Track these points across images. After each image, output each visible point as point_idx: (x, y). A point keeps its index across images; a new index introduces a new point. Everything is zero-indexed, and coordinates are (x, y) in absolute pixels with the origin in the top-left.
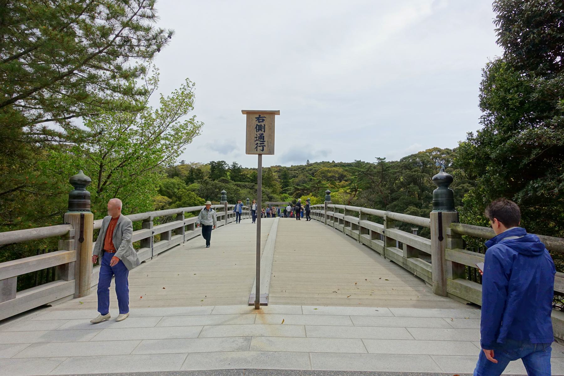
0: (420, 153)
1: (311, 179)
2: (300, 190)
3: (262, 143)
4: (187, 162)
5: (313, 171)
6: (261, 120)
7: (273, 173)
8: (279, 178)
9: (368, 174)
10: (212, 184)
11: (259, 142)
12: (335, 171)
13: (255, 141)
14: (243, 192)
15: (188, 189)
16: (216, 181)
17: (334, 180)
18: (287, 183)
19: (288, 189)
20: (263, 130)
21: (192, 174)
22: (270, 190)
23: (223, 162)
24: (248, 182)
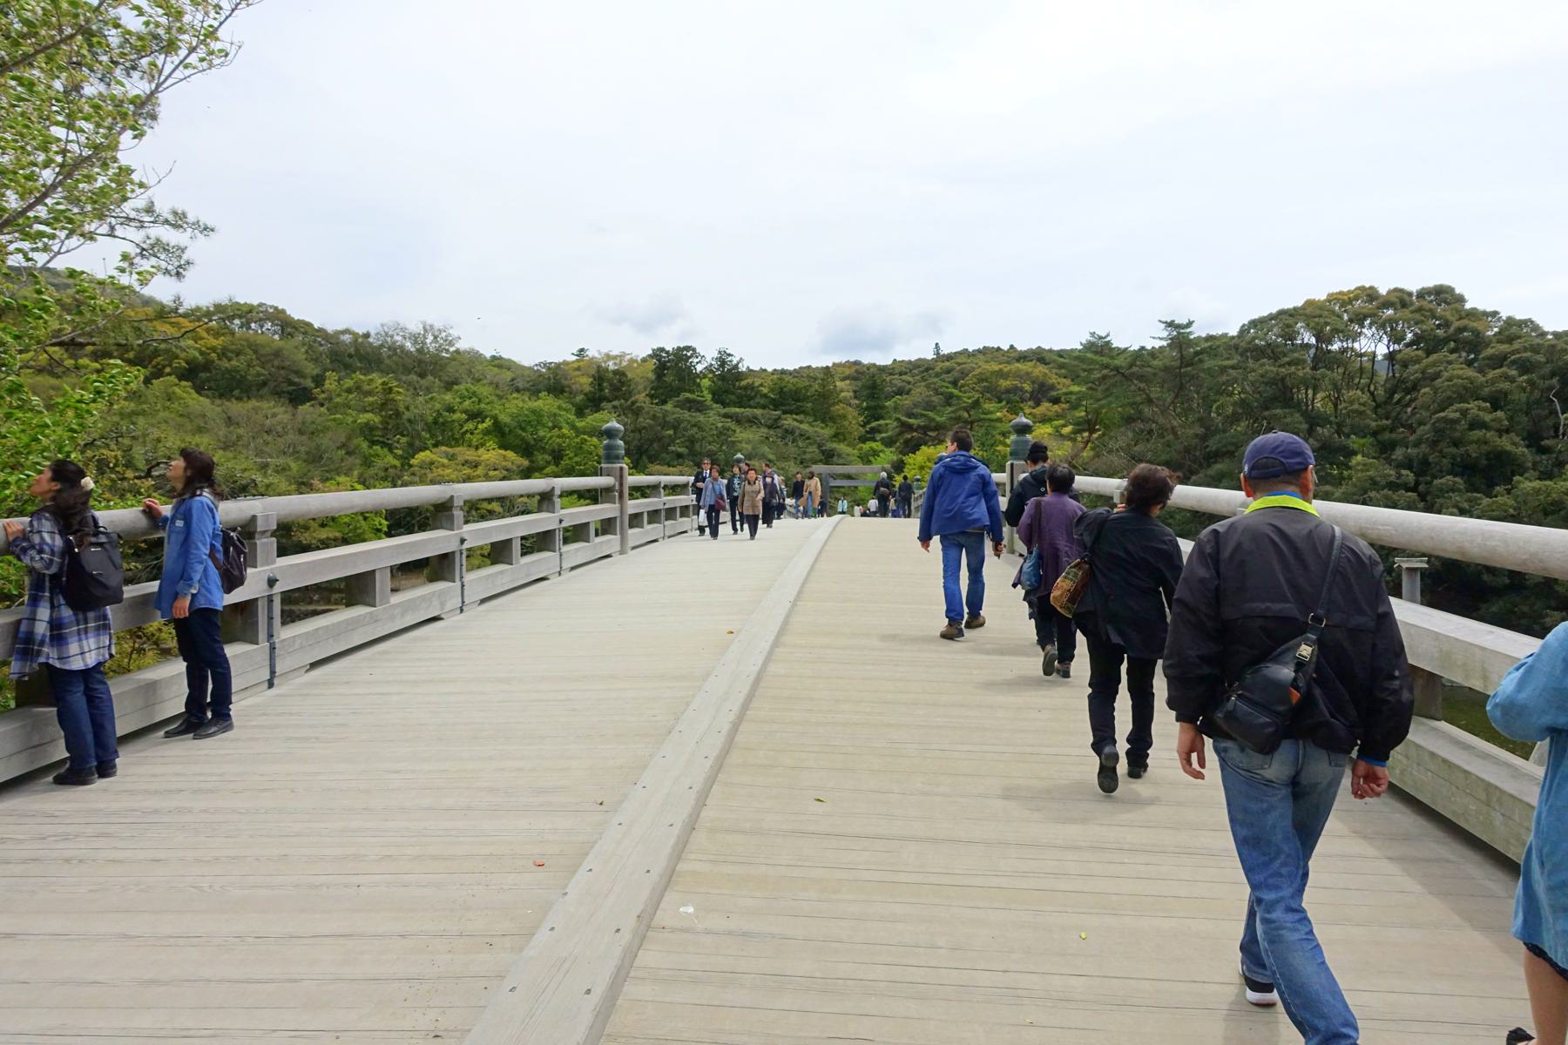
0: (1309, 303)
1: (951, 396)
2: (916, 431)
4: (592, 353)
5: (955, 374)
7: (838, 384)
8: (856, 397)
9: (1132, 374)
10: (652, 413)
12: (1022, 373)
14: (746, 437)
15: (584, 427)
16: (669, 407)
17: (1017, 398)
18: (879, 411)
19: (880, 425)
21: (599, 385)
22: (827, 432)
23: (688, 348)
24: (764, 407)
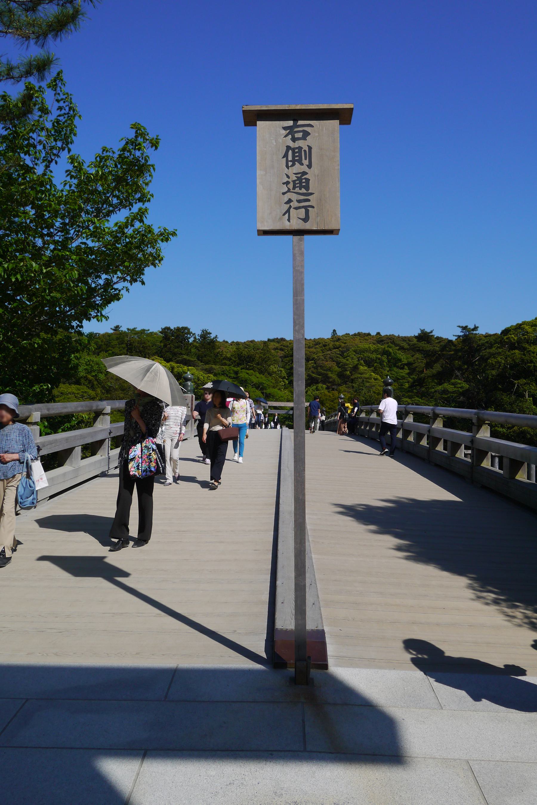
3: (302, 197)
6: (300, 135)
11: (294, 197)
13: (284, 194)
20: (306, 162)
23: (186, 328)
